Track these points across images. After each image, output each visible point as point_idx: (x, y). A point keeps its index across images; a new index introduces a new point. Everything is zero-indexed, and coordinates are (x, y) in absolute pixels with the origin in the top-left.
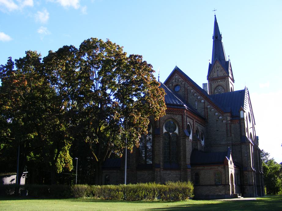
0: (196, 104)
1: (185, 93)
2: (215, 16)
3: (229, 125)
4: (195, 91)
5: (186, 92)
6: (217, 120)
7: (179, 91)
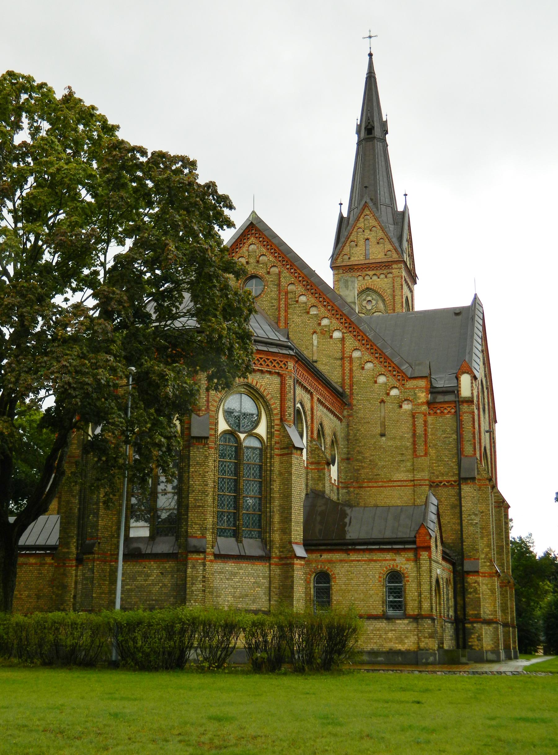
0: (315, 343)
1: (279, 304)
2: (370, 55)
3: (420, 422)
4: (313, 300)
5: (282, 302)
6: (382, 401)
7: (260, 294)
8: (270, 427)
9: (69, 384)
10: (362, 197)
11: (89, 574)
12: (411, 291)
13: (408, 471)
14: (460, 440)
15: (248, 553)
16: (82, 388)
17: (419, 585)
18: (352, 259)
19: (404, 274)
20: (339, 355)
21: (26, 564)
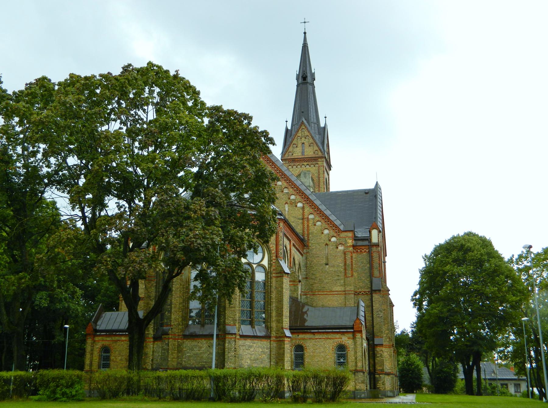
0: (287, 209)
2: (305, 33)
3: (348, 256)
4: (285, 184)
6: (327, 244)
8: (270, 260)
9: (200, 244)
10: (300, 118)
11: (165, 347)
12: (328, 175)
13: (341, 285)
14: (371, 268)
15: (258, 335)
16: (206, 246)
17: (356, 352)
18: (294, 155)
19: (325, 164)
20: (301, 217)
21: (119, 341)
